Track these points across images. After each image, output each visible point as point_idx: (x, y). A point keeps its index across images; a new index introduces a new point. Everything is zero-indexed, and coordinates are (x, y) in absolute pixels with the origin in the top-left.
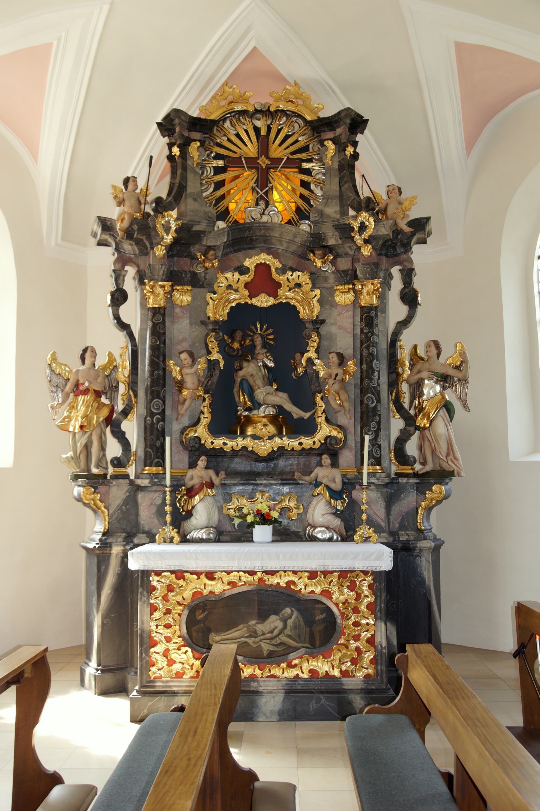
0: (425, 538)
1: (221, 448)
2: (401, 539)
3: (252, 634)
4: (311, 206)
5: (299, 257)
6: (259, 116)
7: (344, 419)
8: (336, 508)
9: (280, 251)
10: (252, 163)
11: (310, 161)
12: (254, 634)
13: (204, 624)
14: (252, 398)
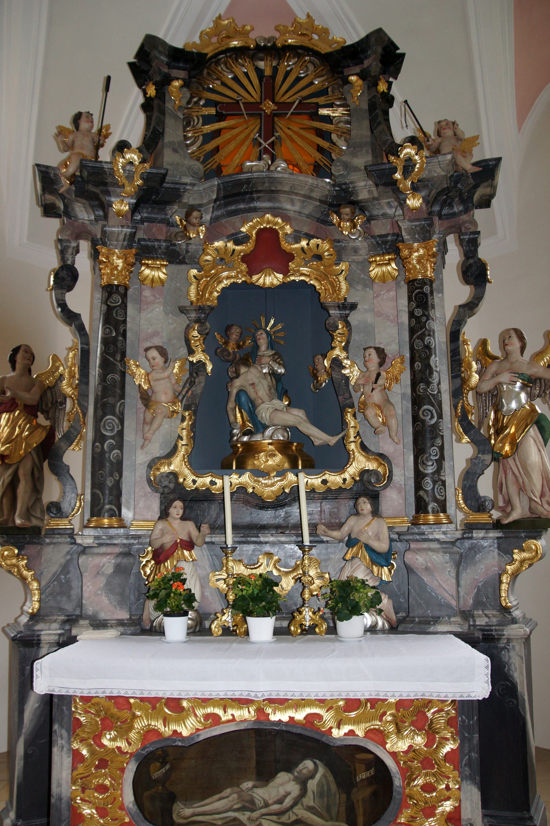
0: (514, 621)
1: (208, 489)
2: (478, 623)
3: (247, 804)
4: (333, 160)
5: (317, 221)
6: (261, 55)
7: (387, 447)
8: (381, 579)
9: (291, 214)
10: (253, 109)
11: (330, 105)
12: (249, 805)
13: (163, 786)
14: (253, 415)
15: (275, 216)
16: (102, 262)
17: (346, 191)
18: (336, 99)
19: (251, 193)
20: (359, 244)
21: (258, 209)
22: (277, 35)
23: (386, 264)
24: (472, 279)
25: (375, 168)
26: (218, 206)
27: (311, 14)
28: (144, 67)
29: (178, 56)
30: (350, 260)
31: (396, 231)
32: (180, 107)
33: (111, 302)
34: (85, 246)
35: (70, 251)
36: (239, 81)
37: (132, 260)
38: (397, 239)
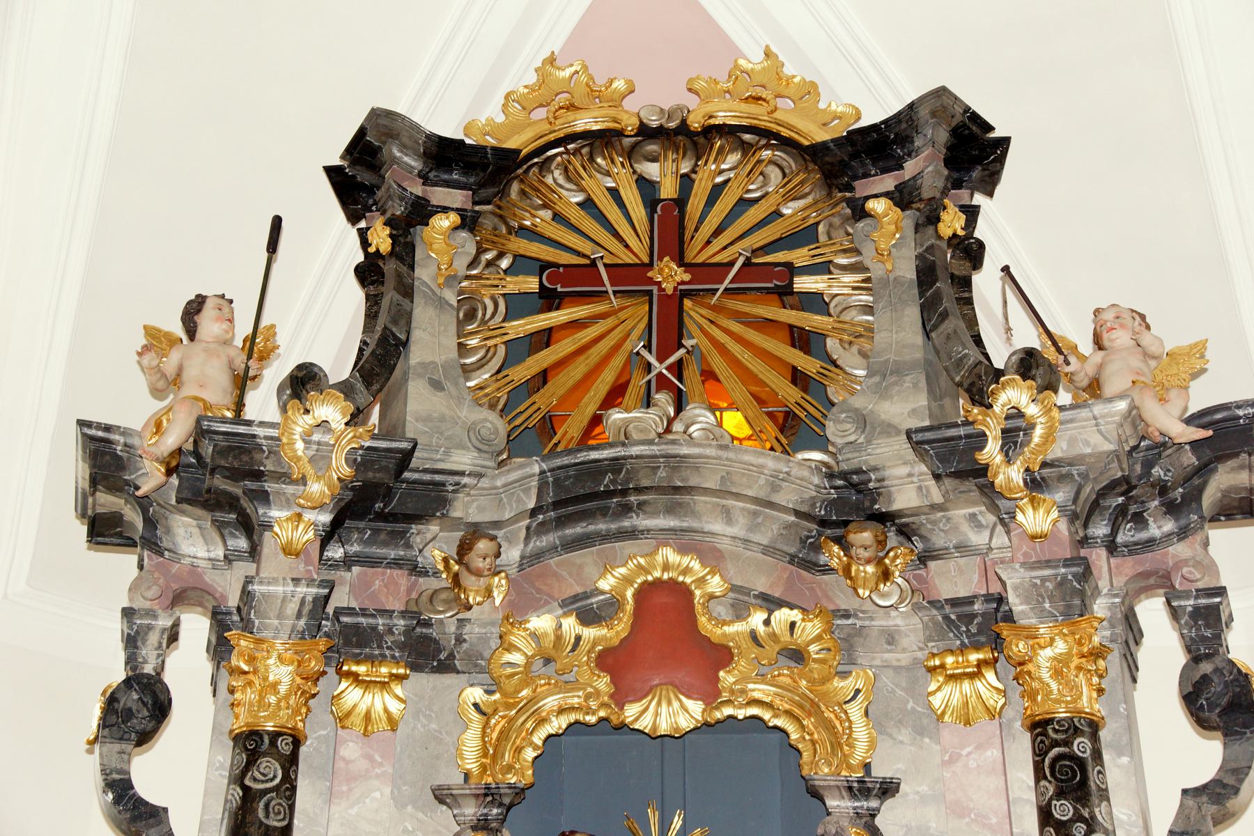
6: (652, 148)
9: (725, 545)
10: (631, 276)
11: (824, 268)
15: (683, 550)
16: (236, 672)
17: (860, 488)
18: (836, 253)
19: (624, 492)
20: (899, 622)
21: (642, 532)
22: (691, 102)
23: (972, 676)
24: (1214, 716)
25: (929, 435)
26: (542, 524)
27: (774, 49)
28: (364, 177)
29: (445, 156)
30: (877, 662)
31: (995, 588)
32: (451, 280)
33: (255, 780)
34: (196, 627)
35: (153, 638)
36: (594, 211)
37: (314, 665)
38: (997, 610)
